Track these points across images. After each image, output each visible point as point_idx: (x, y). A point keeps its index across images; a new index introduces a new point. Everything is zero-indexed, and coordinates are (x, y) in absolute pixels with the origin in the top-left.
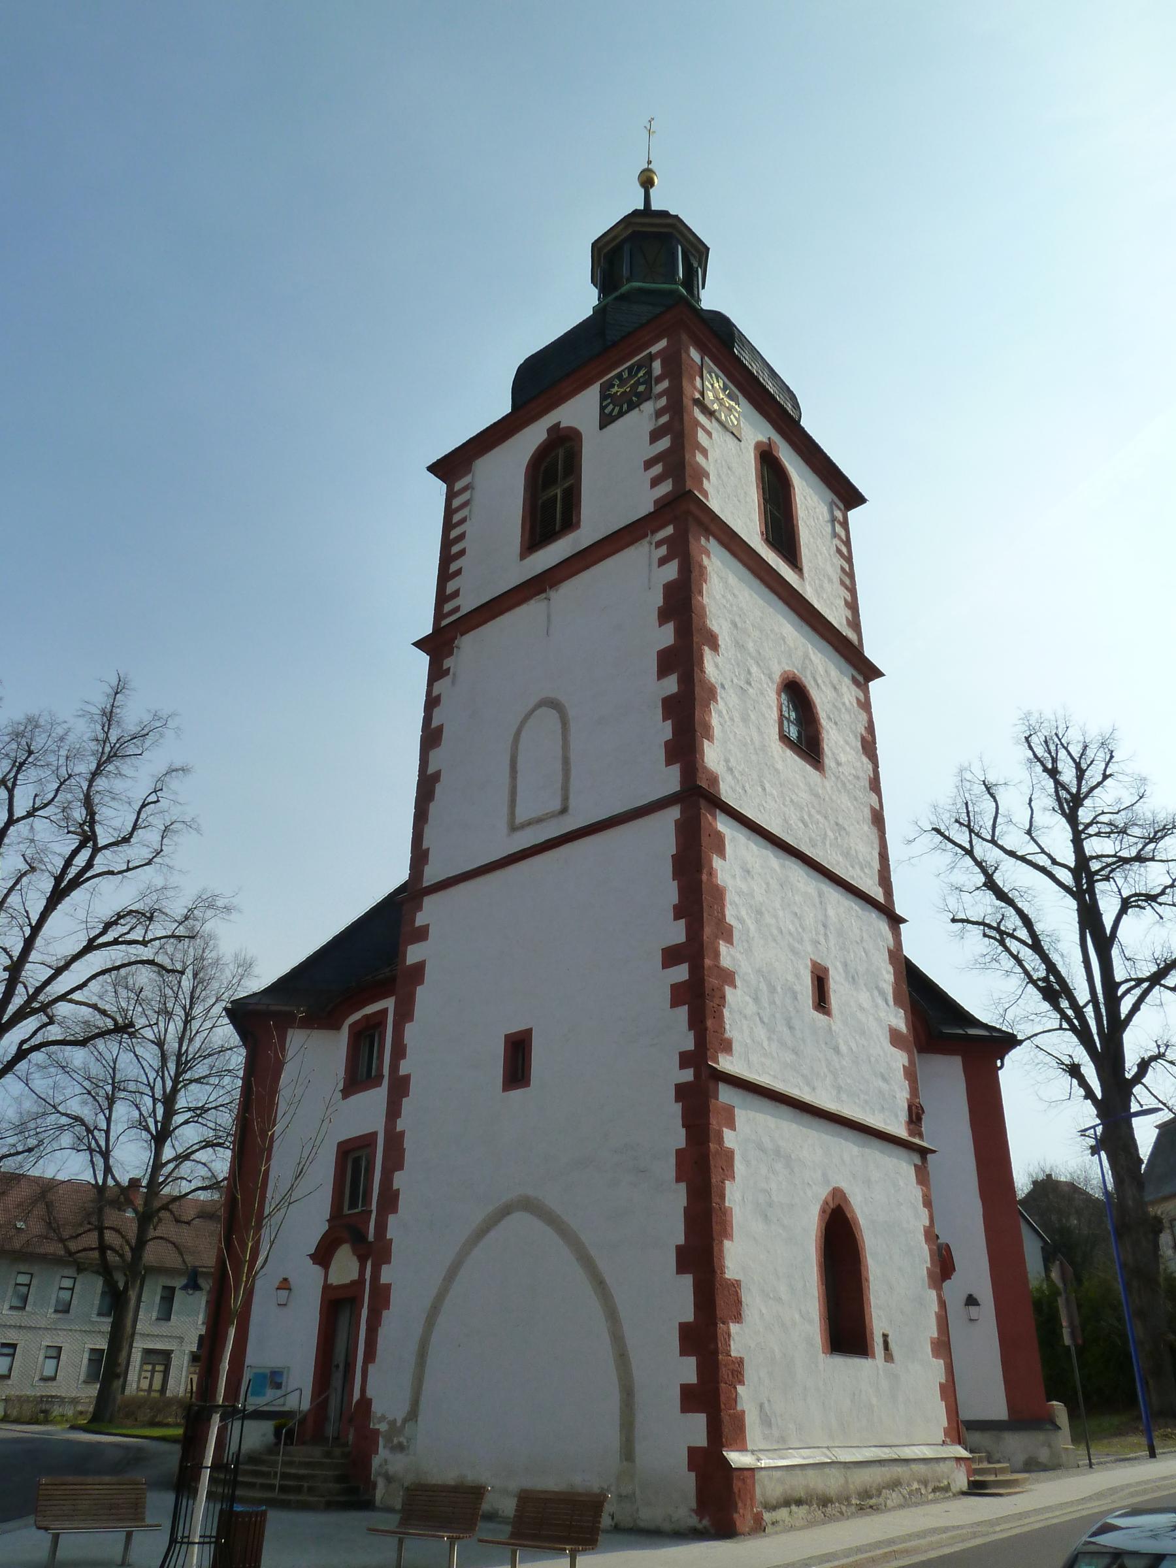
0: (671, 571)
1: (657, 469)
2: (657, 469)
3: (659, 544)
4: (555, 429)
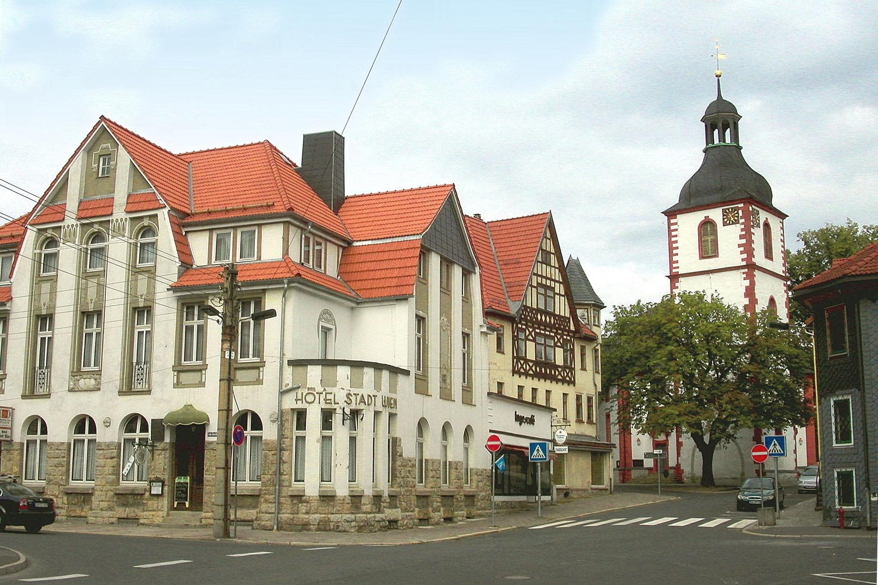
0: (747, 283)
1: (742, 249)
2: (742, 249)
3: (743, 273)
4: (707, 217)
